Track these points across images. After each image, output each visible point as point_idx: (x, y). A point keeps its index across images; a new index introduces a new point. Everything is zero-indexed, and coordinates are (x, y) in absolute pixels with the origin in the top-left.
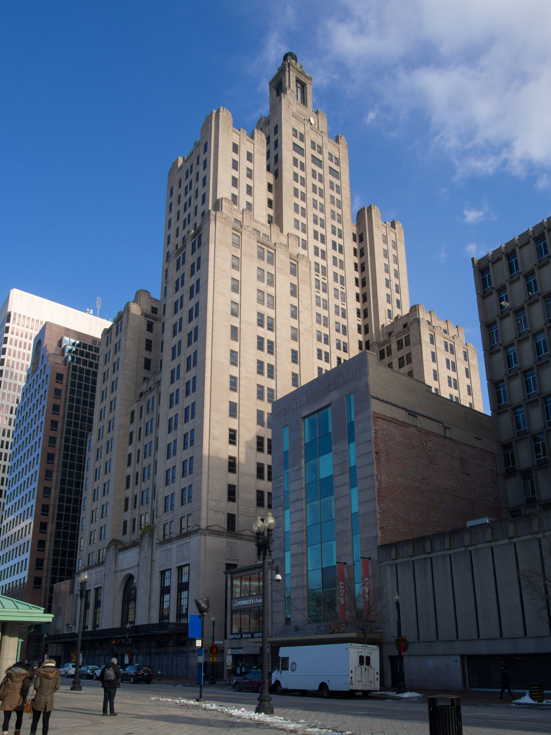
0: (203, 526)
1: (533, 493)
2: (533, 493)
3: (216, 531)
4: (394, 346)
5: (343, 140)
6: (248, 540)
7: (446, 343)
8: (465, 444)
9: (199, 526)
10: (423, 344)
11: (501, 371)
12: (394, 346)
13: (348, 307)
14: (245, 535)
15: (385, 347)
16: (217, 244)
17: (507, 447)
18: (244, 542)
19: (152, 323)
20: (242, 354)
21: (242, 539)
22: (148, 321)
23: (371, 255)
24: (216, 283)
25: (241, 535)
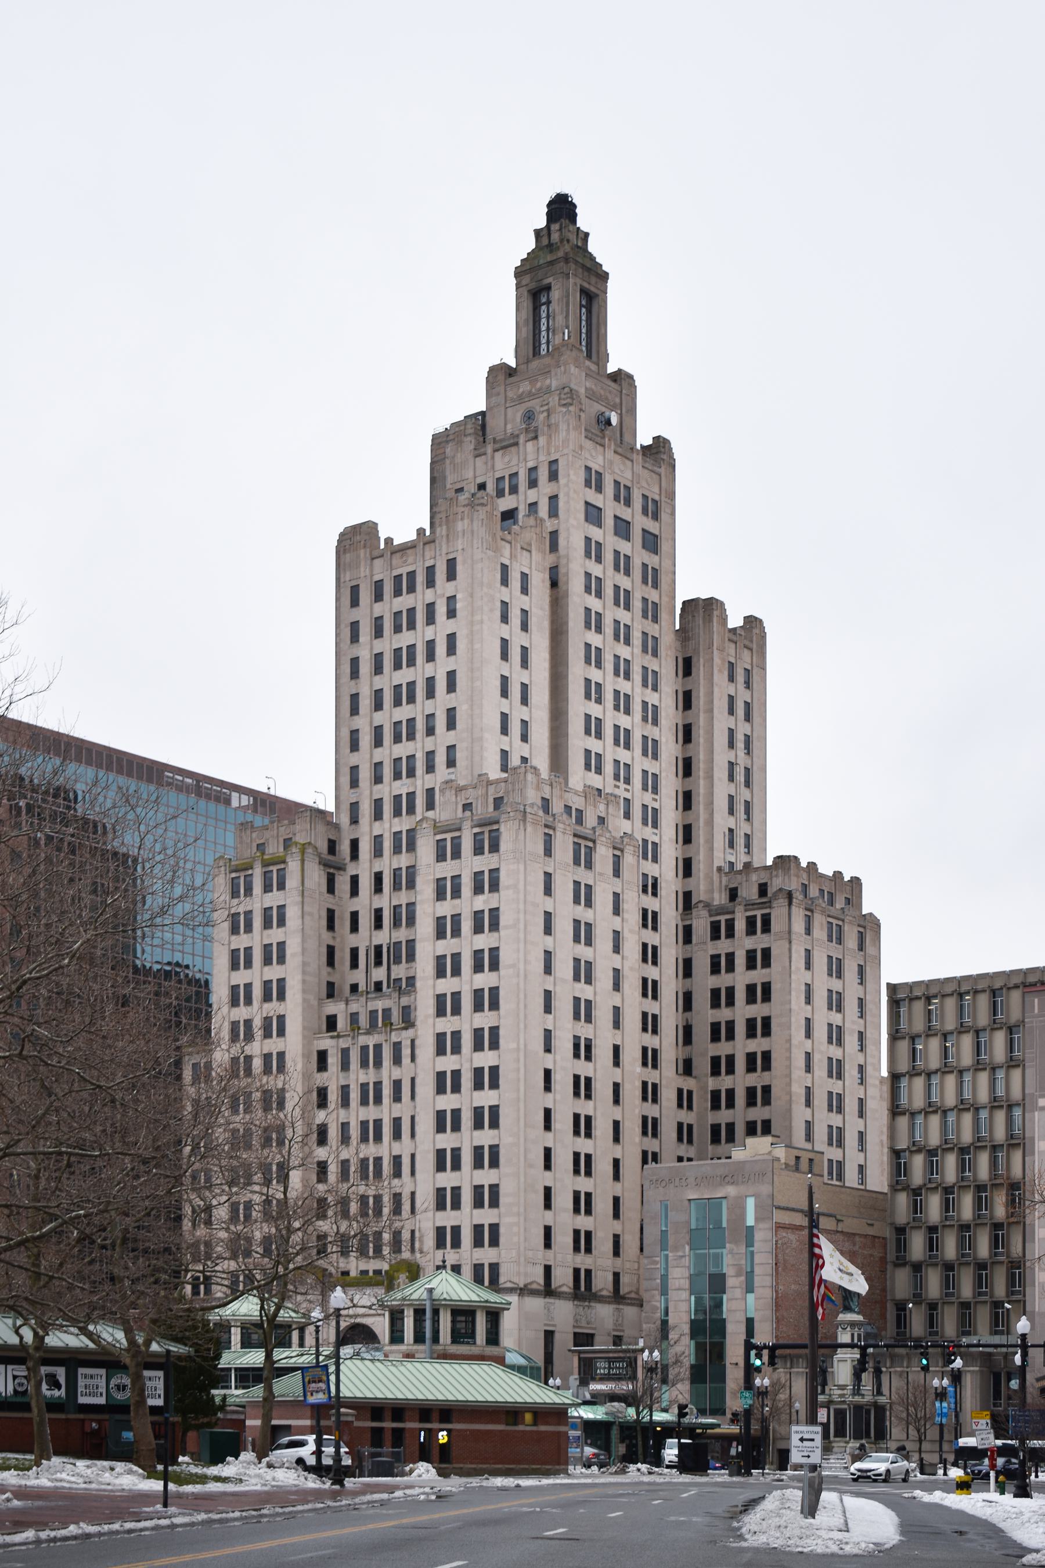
15: (723, 918)
22: (328, 873)
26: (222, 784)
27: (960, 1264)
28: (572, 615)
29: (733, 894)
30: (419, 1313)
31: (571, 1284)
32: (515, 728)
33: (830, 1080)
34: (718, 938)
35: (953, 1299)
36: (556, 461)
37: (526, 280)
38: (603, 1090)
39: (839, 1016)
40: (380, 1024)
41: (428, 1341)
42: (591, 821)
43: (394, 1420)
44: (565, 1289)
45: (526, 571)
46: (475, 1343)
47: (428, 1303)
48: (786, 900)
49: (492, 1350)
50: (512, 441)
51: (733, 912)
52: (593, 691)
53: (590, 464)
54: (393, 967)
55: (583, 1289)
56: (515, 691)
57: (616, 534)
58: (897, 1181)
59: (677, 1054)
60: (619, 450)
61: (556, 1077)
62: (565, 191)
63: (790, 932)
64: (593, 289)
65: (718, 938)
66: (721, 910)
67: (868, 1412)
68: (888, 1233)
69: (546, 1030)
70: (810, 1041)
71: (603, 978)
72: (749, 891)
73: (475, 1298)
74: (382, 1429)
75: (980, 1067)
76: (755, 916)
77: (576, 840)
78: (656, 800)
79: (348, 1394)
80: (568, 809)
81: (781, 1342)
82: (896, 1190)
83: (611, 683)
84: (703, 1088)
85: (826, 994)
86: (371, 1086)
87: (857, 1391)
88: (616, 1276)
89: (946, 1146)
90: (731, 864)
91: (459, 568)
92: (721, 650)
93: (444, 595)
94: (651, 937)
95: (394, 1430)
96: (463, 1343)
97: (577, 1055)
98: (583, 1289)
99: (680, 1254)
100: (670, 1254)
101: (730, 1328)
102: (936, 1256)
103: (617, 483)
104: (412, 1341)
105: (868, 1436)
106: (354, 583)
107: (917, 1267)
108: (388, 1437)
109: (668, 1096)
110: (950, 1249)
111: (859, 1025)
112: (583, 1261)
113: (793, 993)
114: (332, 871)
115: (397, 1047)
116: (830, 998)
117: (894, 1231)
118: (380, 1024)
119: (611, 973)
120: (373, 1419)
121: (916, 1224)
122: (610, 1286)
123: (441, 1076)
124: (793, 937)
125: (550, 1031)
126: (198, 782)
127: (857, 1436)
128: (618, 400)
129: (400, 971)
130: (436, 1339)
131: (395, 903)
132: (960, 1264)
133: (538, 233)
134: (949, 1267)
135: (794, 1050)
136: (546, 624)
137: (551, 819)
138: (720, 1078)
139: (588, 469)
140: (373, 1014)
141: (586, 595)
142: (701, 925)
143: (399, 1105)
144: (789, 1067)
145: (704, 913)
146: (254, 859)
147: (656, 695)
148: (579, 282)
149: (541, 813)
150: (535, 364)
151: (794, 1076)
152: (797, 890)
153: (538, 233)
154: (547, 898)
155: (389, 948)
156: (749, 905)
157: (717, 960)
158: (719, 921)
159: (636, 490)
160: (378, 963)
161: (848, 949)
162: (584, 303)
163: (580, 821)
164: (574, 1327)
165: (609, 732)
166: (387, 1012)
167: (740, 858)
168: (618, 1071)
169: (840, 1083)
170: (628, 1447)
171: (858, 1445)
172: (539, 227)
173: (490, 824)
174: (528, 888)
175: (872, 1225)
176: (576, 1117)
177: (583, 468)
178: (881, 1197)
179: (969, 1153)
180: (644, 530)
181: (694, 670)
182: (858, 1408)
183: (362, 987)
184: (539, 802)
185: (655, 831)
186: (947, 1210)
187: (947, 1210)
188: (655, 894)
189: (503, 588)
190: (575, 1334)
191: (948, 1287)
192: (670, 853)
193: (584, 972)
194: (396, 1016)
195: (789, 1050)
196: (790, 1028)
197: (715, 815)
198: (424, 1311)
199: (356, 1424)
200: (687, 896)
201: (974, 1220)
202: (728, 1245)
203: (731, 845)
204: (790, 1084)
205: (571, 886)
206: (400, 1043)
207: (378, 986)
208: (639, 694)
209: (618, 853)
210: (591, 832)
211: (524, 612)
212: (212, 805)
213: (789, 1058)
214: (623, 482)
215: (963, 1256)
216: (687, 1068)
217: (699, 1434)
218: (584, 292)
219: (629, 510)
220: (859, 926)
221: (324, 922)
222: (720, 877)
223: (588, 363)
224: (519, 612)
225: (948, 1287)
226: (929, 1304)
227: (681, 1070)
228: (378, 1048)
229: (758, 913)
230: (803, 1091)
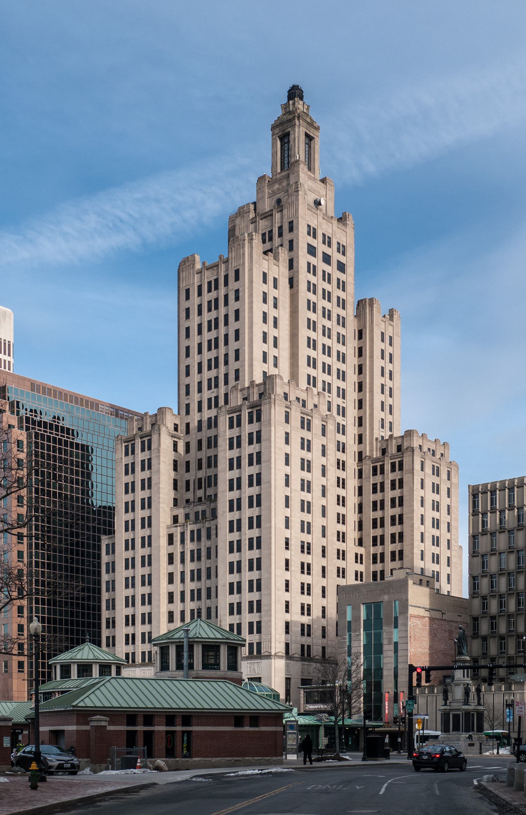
0: (273, 653)
1: (487, 650)
2: (487, 650)
3: (280, 656)
4: (388, 467)
5: (350, 222)
6: (297, 661)
7: (433, 466)
8: (452, 621)
9: (271, 653)
10: (415, 474)
11: (478, 571)
12: (388, 467)
13: (348, 422)
14: (295, 657)
15: (378, 464)
16: (277, 426)
17: (475, 619)
18: (295, 662)
19: (177, 442)
20: (292, 519)
21: (293, 660)
22: (174, 441)
23: (370, 358)
24: (277, 461)
25: (294, 657)
26: (129, 411)
27: (508, 636)
28: (300, 302)
29: (384, 452)
30: (179, 649)
31: (300, 653)
32: (271, 360)
33: (433, 546)
34: (376, 474)
35: (504, 655)
36: (292, 221)
37: (277, 131)
38: (316, 550)
39: (438, 514)
40: (200, 518)
41: (186, 668)
42: (310, 406)
43: (184, 725)
44: (296, 655)
45: (277, 277)
46: (219, 669)
47: (185, 640)
48: (411, 453)
49: (232, 674)
50: (270, 213)
51: (384, 461)
52: (312, 344)
53: (310, 224)
54: (208, 489)
55: (306, 655)
56: (271, 340)
58: (474, 592)
61: (292, 543)
62: (296, 83)
63: (413, 469)
64: (311, 134)
65: (376, 474)
66: (377, 460)
67: (473, 715)
68: (469, 620)
69: (286, 517)
70: (423, 526)
71: (317, 489)
72: (392, 450)
75: (520, 528)
76: (395, 462)
77: (302, 415)
78: (344, 403)
80: (298, 399)
81: (433, 665)
82: (473, 597)
83: (322, 340)
84: (368, 552)
85: (431, 502)
86: (196, 551)
87: (466, 703)
88: (324, 648)
89: (501, 572)
90: (382, 437)
92: (378, 325)
93: (233, 289)
94: (342, 492)
95: (145, 732)
96: (210, 669)
97: (303, 531)
98: (306, 655)
100: (352, 634)
101: (385, 673)
102: (495, 632)
103: (324, 235)
104: (174, 668)
105: (473, 730)
106: (187, 288)
107: (485, 639)
108: (140, 740)
109: (350, 557)
110: (502, 629)
111: (448, 519)
112: (306, 640)
113: (415, 501)
114: (176, 440)
115: (209, 530)
116: (433, 504)
117: (472, 620)
118: (200, 518)
119: (321, 488)
120: (128, 724)
121: (485, 615)
122: (320, 654)
124: (415, 471)
125: (288, 518)
126: (117, 410)
127: (467, 730)
128: (325, 193)
129: (210, 492)
130: (191, 666)
131: (208, 455)
132: (508, 636)
134: (502, 638)
135: (415, 531)
136: (288, 305)
137: (289, 404)
138: (377, 547)
139: (309, 226)
140: (197, 513)
141: (308, 292)
142: (368, 468)
143: (210, 561)
144: (413, 540)
145: (369, 462)
146: (135, 435)
147: (344, 347)
148: (305, 130)
149: (283, 400)
151: (415, 545)
152: (417, 447)
154: (287, 446)
155: (205, 479)
156: (392, 457)
157: (375, 486)
158: (377, 466)
159: (334, 239)
160: (200, 488)
161: (443, 479)
162: (307, 142)
163: (304, 405)
164: (301, 676)
165: (320, 366)
166: (204, 512)
167: (387, 434)
168: (325, 539)
169: (438, 548)
170: (329, 739)
171: (468, 736)
173: (257, 406)
174: (276, 440)
175: (461, 616)
176: (302, 564)
177: (306, 226)
178: (465, 601)
179: (486, 599)
180: (338, 261)
181: (363, 336)
182: (467, 714)
184: (283, 395)
185: (344, 418)
186: (501, 607)
187: (501, 607)
188: (343, 452)
189: (264, 285)
190: (302, 679)
191: (501, 649)
192: (352, 430)
193: (306, 486)
194: (208, 514)
195: (413, 531)
196: (413, 520)
197: (375, 411)
198: (182, 646)
200: (360, 454)
201: (516, 611)
202: (384, 628)
203: (383, 427)
204: (413, 549)
205: (300, 440)
206: (210, 528)
207: (200, 499)
208: (336, 347)
209: (325, 424)
210: (311, 412)
211: (275, 298)
212: (123, 421)
213: (413, 535)
215: (510, 631)
216: (360, 543)
217: (371, 731)
218: (307, 135)
219: (331, 249)
221: (172, 467)
222: (377, 443)
223: (309, 173)
224: (272, 298)
225: (501, 649)
226: (491, 658)
227: (357, 544)
228: (199, 531)
229: (397, 461)
230: (420, 552)
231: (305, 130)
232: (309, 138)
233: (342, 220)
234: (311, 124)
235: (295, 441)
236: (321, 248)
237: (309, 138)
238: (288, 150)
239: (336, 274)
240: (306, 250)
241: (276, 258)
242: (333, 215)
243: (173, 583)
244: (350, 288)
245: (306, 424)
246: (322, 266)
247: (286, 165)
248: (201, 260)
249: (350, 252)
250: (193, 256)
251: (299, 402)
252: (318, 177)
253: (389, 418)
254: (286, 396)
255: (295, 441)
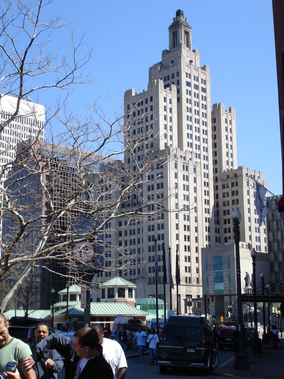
42: (188, 159)
57: (194, 88)
59: (215, 219)
60: (195, 68)
73: (125, 284)
74: (103, 324)
79: (94, 313)
91: (153, 98)
99: (211, 271)
123: (149, 226)
133: (174, 19)
148: (184, 29)
150: (174, 49)
153: (174, 19)
172: (174, 17)
180: (202, 87)
183: (131, 204)
199: (78, 322)
214: (196, 76)
220: (247, 180)
231: (184, 29)
232: (187, 33)
233: (204, 68)
234: (187, 26)
235: (180, 177)
236: (194, 82)
237: (187, 33)
238: (177, 41)
239: (201, 94)
240: (185, 84)
241: (171, 90)
242: (199, 67)
243: (149, 257)
244: (209, 99)
245: (185, 168)
246: (194, 91)
247: (176, 45)
248: (135, 90)
249: (208, 83)
250: (131, 90)
251: (182, 158)
252: (192, 49)
253: (231, 160)
254: (175, 156)
255: (180, 177)
